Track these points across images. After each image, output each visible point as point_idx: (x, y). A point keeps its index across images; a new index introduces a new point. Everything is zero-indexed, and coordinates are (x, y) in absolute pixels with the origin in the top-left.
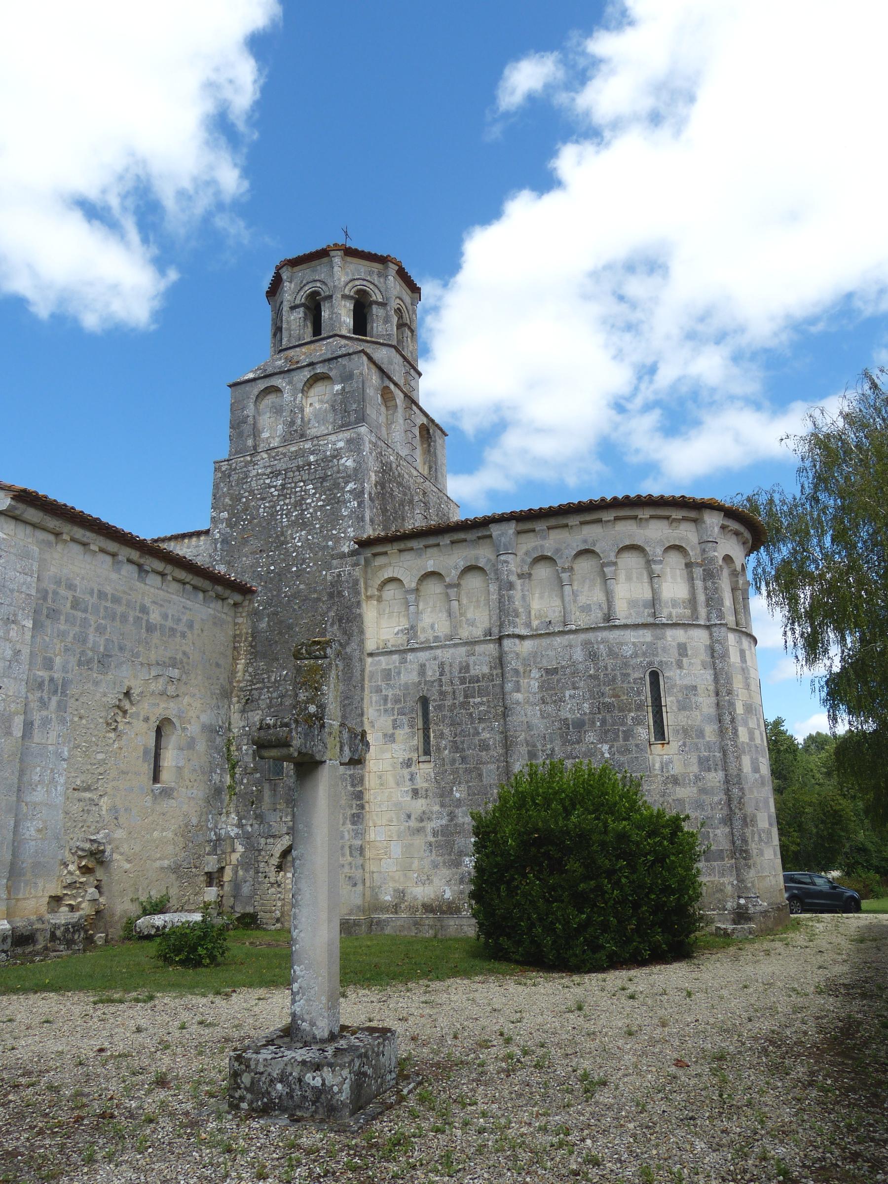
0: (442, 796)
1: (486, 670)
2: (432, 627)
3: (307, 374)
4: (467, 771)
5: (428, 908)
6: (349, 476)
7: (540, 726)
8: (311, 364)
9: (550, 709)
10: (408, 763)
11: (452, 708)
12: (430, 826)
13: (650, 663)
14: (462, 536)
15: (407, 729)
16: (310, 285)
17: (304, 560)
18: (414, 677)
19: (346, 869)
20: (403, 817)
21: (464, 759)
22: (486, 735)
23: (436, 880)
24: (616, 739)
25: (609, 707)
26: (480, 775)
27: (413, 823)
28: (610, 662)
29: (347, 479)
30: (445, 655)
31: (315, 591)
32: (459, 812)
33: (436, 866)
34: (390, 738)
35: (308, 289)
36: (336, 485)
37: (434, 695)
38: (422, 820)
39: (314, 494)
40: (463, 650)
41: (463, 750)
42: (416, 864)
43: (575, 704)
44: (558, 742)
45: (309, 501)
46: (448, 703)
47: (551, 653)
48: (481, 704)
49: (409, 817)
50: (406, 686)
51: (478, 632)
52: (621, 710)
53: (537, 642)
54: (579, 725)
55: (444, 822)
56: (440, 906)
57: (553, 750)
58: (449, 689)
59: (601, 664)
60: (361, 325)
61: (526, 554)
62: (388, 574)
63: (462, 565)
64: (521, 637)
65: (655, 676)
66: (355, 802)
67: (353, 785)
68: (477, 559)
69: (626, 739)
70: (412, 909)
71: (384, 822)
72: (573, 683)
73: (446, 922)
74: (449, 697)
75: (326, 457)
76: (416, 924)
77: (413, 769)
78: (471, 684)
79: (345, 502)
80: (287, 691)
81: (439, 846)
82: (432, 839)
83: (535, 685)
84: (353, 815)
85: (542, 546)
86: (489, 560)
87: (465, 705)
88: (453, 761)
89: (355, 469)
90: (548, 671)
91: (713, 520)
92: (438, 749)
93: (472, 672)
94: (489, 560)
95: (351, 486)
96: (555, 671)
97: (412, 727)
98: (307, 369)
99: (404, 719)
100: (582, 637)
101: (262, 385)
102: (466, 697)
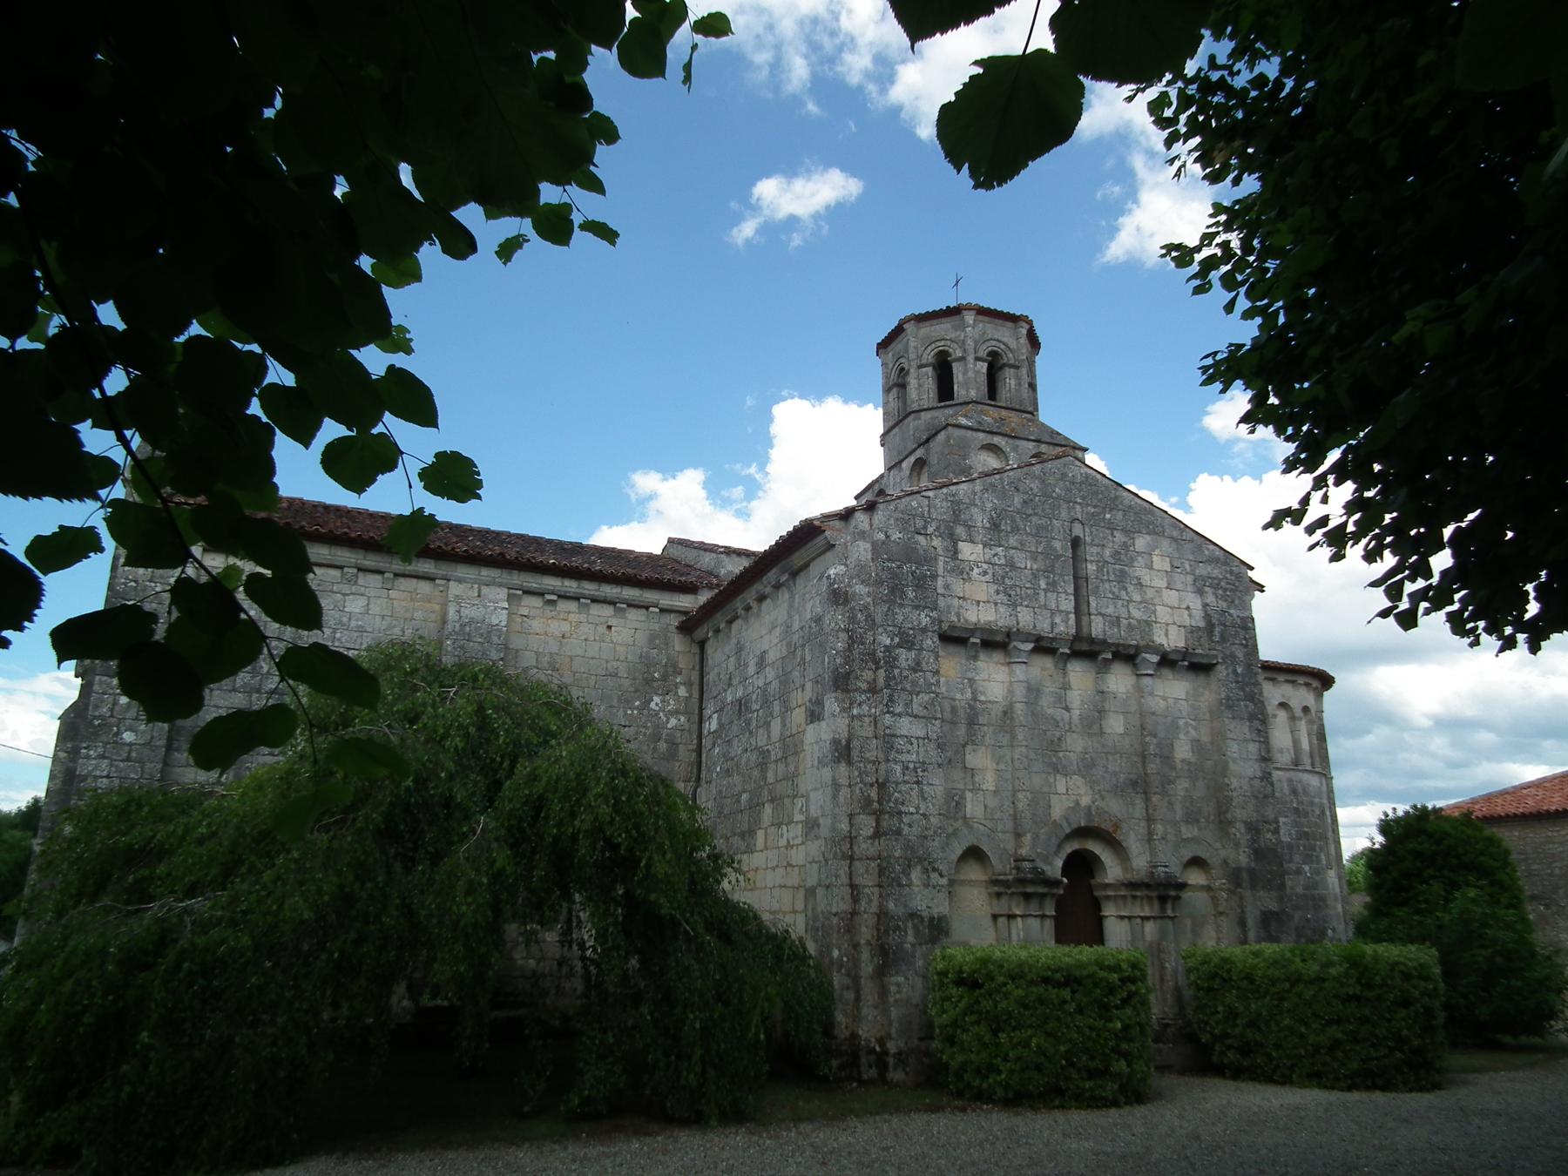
25: (1306, 835)
35: (991, 346)
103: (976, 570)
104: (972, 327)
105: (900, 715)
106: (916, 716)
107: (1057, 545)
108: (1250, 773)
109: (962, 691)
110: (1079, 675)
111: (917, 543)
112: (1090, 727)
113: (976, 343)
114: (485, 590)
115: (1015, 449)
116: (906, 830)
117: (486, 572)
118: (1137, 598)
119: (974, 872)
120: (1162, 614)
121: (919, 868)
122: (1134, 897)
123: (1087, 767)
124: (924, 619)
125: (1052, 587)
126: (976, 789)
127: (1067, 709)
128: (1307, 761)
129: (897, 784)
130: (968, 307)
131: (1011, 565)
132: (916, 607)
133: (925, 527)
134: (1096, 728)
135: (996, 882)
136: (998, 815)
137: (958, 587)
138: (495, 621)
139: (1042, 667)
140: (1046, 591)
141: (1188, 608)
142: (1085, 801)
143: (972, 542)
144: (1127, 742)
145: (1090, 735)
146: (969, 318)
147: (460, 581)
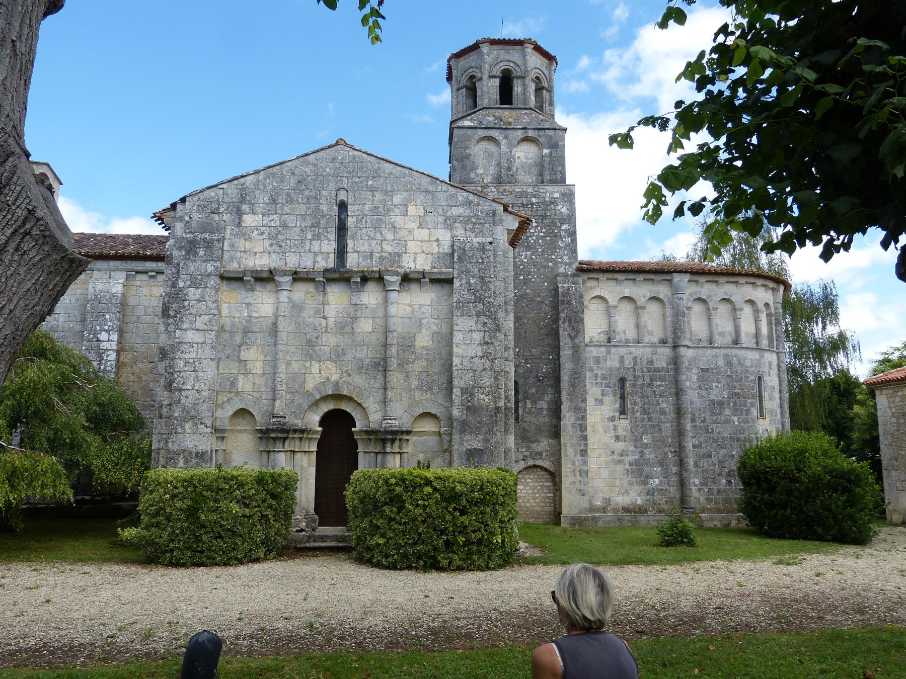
0: (635, 441)
1: (664, 365)
2: (624, 332)
3: (520, 134)
4: (653, 427)
5: (626, 510)
6: (564, 219)
7: (698, 402)
8: (525, 128)
9: (704, 393)
10: (612, 419)
11: (642, 386)
12: (627, 459)
13: (758, 372)
14: (652, 276)
15: (611, 397)
16: (505, 63)
17: (529, 273)
18: (616, 364)
19: (577, 485)
20: (609, 453)
21: (650, 419)
22: (664, 405)
23: (631, 493)
24: (741, 414)
25: (738, 395)
26: (660, 430)
27: (616, 457)
28: (739, 368)
29: (563, 221)
30: (638, 351)
31: (539, 296)
32: (647, 451)
33: (631, 484)
34: (600, 402)
35: (503, 66)
36: (553, 223)
37: (630, 376)
38: (622, 455)
39: (537, 227)
40: (649, 350)
41: (649, 413)
42: (618, 482)
43: (718, 392)
44: (708, 413)
45: (532, 231)
46: (640, 383)
47: (705, 359)
48: (661, 385)
49: (613, 453)
50: (611, 369)
51: (655, 339)
52: (744, 398)
53: (696, 350)
54: (721, 404)
55: (636, 457)
56: (634, 509)
57: (705, 418)
58: (640, 374)
59: (734, 369)
60: (506, 95)
61: (690, 295)
62: (597, 293)
63: (648, 295)
64: (688, 347)
65: (760, 378)
66: (583, 442)
67: (581, 431)
68: (659, 293)
69: (747, 415)
70: (615, 510)
71: (596, 455)
72: (718, 379)
73: (639, 518)
74: (640, 379)
75: (545, 202)
76: (619, 519)
77: (616, 423)
78: (654, 372)
79: (561, 237)
80: (520, 363)
81: (633, 472)
82: (629, 468)
83: (695, 378)
84: (582, 451)
85: (700, 292)
86: (666, 295)
87: (650, 385)
88: (643, 420)
89: (568, 215)
90: (702, 370)
91: (681, 280)
92: (633, 412)
93: (655, 365)
94: (666, 295)
95: (565, 227)
96: (707, 370)
97: (615, 396)
98: (520, 131)
99: (610, 391)
100: (723, 351)
101: (482, 133)
102: (651, 380)
103: (256, 232)
104: (489, 54)
105: (186, 330)
106: (198, 330)
107: (324, 208)
108: (471, 353)
109: (241, 312)
110: (337, 298)
111: (212, 219)
112: (342, 328)
113: (490, 66)
114: (113, 274)
115: (506, 137)
116: (184, 400)
117: (112, 263)
118: (390, 236)
119: (243, 425)
120: (412, 246)
121: (191, 422)
122: (370, 439)
123: (337, 356)
124: (210, 268)
125: (317, 237)
126: (247, 373)
127: (325, 318)
128: (765, 343)
129: (180, 372)
130: (529, 41)
131: (285, 226)
132: (204, 261)
133: (218, 208)
134: (348, 329)
135: (260, 431)
136: (263, 389)
137: (242, 244)
138: (114, 291)
139: (301, 292)
140: (311, 240)
141: (437, 240)
142: (335, 377)
143: (254, 213)
144: (373, 337)
145: (342, 334)
146: (485, 49)
147: (99, 270)
